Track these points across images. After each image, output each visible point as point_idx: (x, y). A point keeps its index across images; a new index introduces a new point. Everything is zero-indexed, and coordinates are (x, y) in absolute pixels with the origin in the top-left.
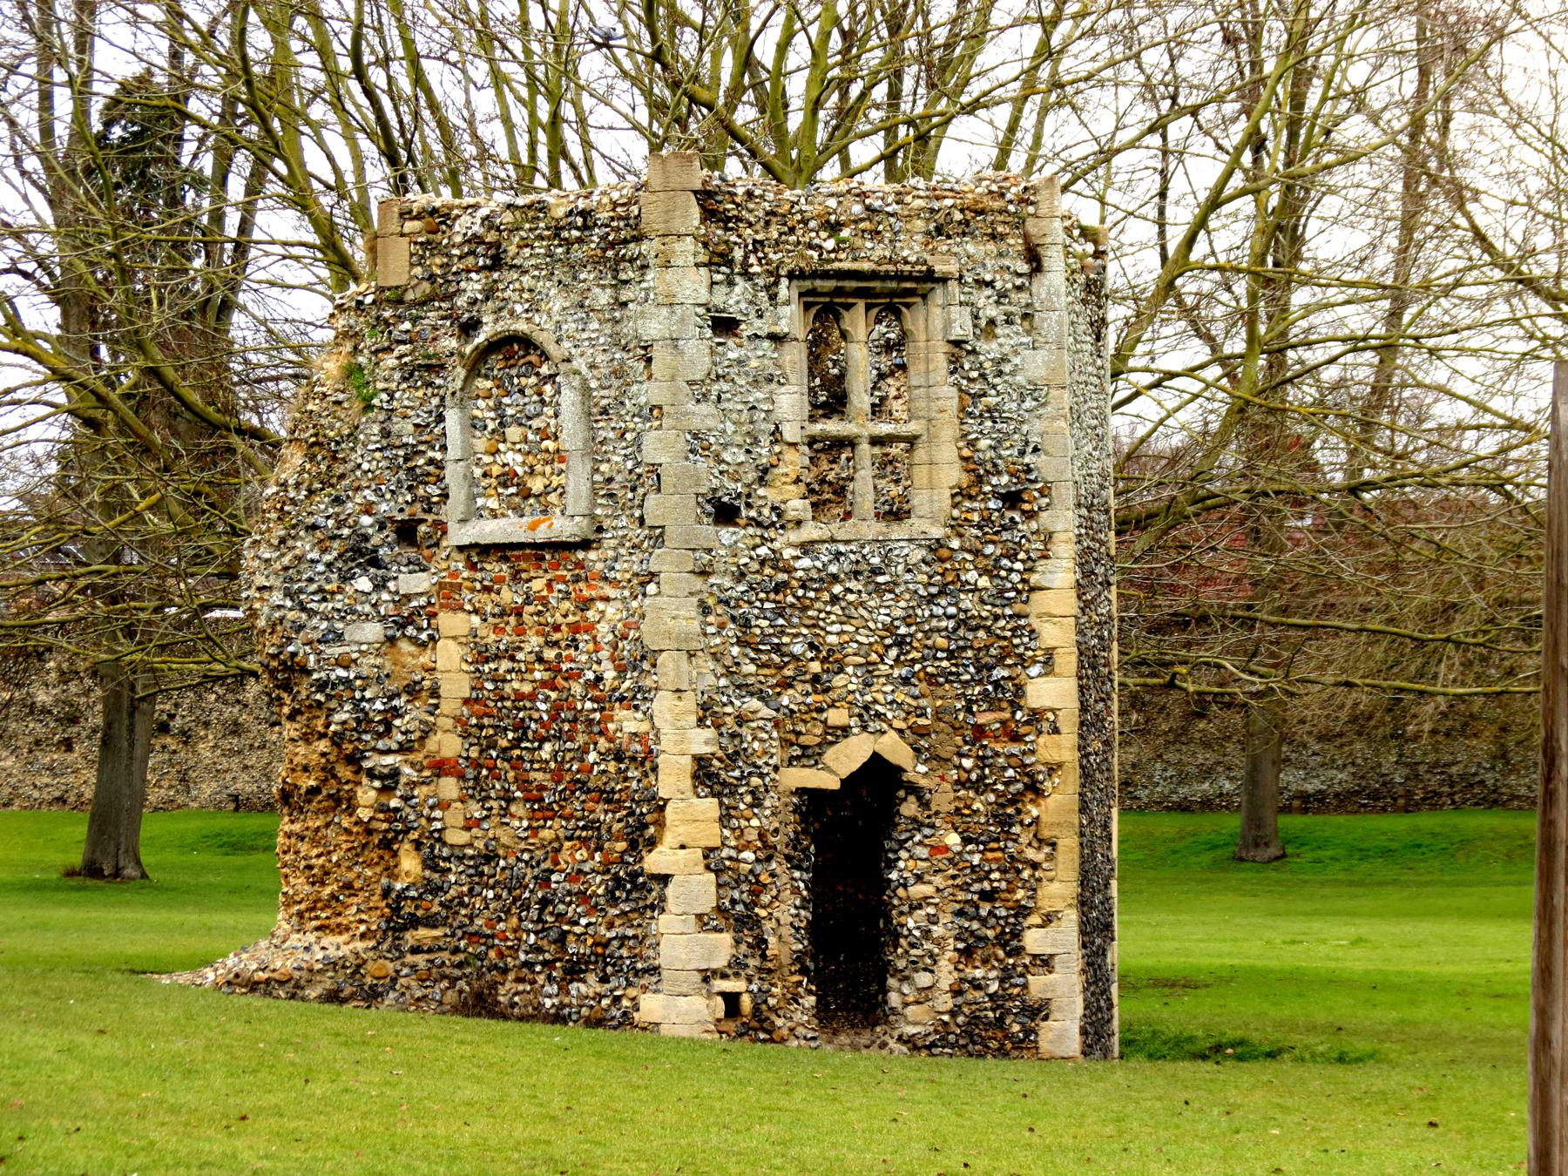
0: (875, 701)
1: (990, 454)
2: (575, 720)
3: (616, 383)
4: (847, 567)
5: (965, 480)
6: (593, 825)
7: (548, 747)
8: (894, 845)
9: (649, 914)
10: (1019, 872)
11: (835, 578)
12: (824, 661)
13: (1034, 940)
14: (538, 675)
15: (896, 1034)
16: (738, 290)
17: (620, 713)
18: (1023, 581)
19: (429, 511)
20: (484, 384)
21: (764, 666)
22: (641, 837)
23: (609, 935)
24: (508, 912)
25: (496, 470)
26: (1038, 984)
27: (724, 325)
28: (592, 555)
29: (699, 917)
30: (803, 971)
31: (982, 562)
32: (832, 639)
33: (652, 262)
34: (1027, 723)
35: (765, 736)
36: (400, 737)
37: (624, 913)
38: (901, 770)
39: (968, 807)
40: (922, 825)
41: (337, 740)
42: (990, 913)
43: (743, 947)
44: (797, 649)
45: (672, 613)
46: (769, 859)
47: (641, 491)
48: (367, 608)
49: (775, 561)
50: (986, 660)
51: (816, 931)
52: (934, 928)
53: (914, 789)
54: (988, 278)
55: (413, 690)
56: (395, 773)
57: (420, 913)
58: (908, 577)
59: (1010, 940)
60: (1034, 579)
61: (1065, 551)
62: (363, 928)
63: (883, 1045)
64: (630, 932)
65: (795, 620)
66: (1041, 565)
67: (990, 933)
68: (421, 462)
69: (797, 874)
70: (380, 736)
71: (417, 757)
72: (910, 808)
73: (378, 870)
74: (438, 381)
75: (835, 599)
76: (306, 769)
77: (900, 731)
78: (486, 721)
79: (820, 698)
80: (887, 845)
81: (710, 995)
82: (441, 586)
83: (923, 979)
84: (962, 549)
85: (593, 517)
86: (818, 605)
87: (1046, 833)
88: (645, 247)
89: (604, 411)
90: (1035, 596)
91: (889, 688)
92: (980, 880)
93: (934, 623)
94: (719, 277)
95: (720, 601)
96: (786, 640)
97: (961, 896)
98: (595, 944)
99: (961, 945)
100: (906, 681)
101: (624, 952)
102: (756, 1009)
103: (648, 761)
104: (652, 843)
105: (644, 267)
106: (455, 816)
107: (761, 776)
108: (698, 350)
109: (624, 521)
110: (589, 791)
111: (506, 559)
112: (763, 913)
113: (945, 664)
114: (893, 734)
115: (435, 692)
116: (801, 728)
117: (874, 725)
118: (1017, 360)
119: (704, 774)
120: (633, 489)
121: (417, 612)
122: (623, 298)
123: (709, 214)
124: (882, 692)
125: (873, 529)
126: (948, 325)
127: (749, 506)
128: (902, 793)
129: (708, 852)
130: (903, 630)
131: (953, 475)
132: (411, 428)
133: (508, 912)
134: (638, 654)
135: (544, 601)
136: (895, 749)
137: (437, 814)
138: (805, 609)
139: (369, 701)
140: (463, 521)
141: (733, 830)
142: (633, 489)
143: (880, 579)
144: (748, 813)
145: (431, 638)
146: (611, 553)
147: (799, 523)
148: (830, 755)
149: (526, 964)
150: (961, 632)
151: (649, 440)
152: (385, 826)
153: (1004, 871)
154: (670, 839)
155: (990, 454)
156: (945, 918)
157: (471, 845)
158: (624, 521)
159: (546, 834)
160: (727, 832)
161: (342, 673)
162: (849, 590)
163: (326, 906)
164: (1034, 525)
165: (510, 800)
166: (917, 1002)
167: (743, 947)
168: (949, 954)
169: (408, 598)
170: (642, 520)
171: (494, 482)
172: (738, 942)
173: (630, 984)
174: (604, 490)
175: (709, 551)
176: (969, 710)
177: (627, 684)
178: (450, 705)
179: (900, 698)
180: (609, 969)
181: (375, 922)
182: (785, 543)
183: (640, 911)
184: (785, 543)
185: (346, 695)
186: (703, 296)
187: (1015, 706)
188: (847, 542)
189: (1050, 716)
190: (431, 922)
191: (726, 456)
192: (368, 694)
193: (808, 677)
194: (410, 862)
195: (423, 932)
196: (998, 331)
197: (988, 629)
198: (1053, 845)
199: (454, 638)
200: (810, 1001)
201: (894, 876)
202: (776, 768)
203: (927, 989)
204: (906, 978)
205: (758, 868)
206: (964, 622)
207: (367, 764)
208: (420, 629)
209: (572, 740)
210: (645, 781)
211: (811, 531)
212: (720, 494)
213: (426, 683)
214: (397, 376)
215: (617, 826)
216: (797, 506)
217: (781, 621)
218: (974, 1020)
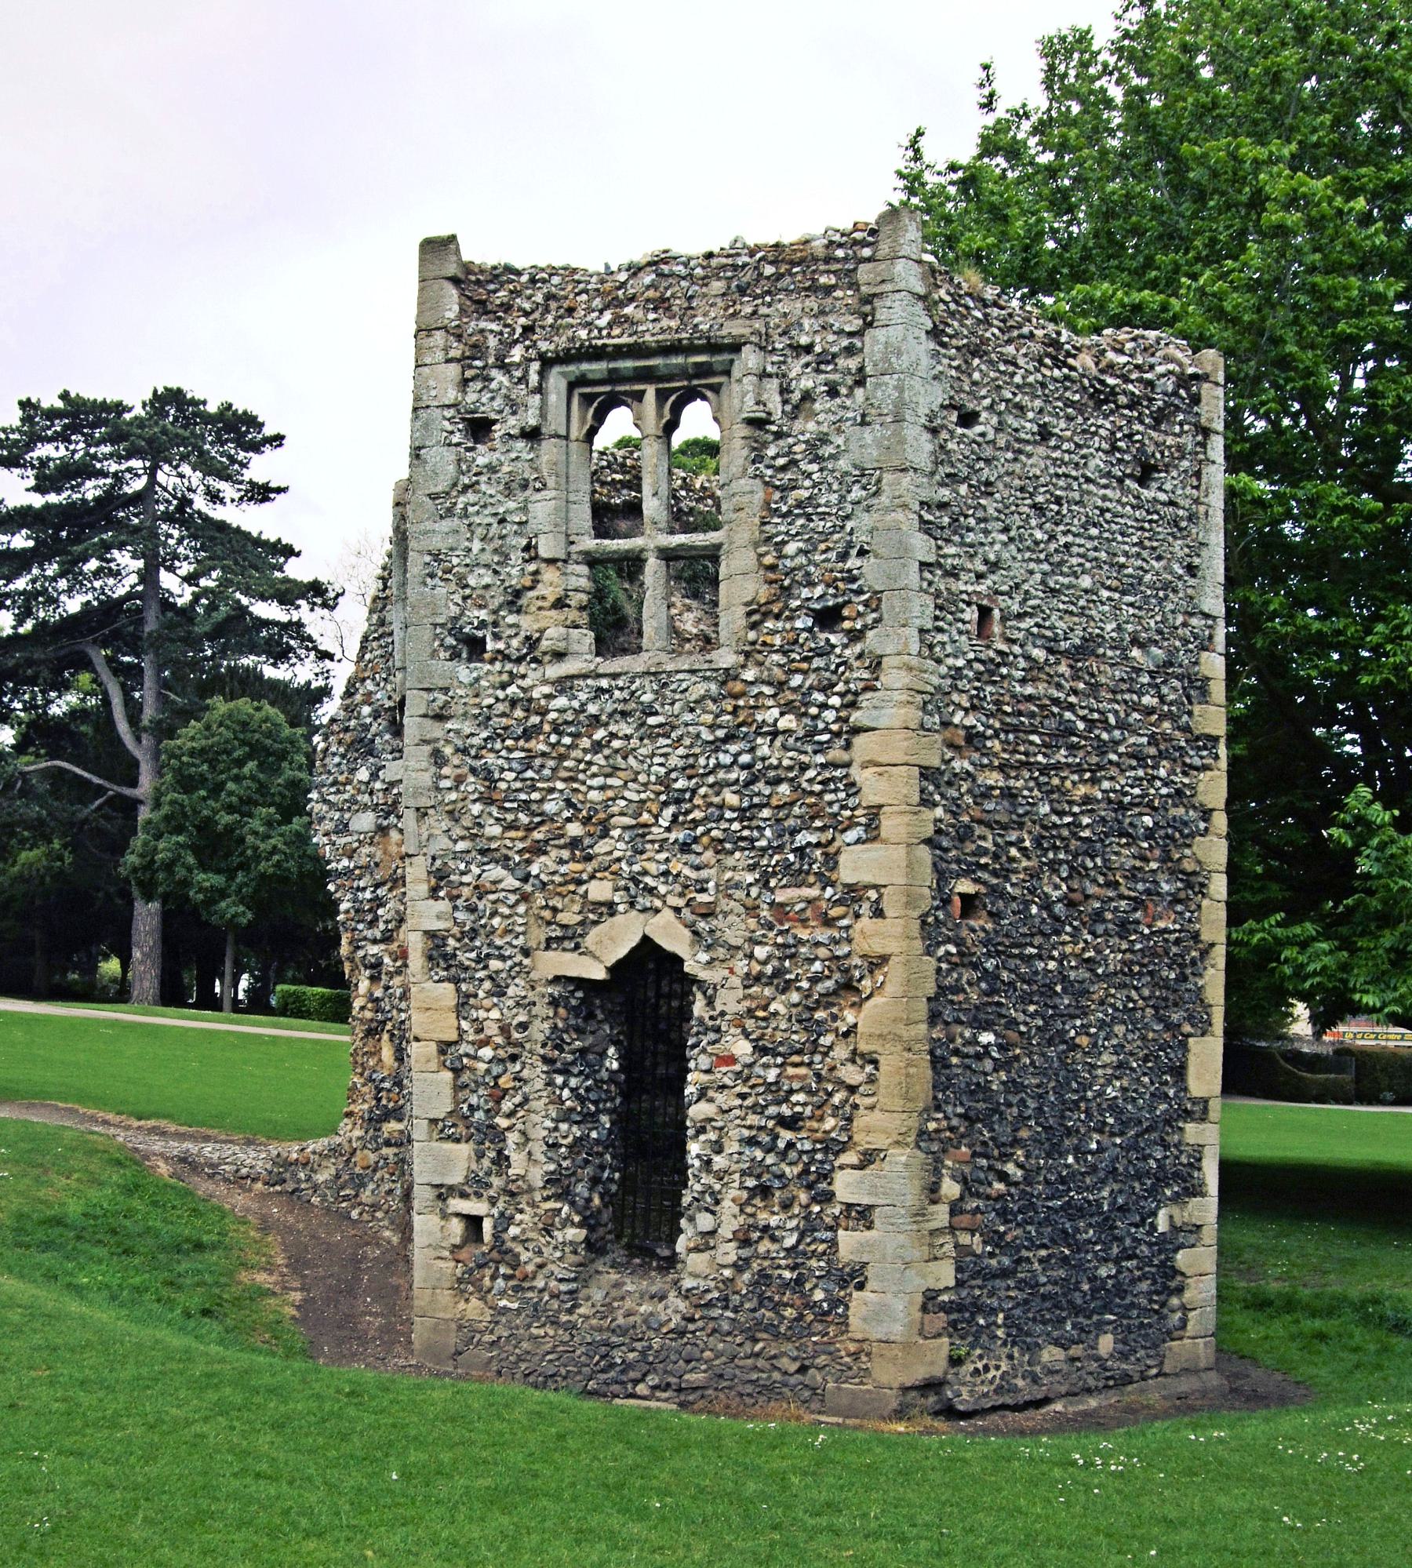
0: (645, 873)
5: (764, 593)
11: (595, 721)
12: (586, 821)
13: (846, 1186)
27: (479, 429)
29: (434, 1121)
30: (565, 1195)
32: (594, 795)
44: (550, 807)
49: (528, 704)
50: (794, 830)
52: (717, 1159)
60: (856, 717)
72: (699, 1008)
75: (597, 747)
77: (677, 910)
79: (578, 867)
81: (445, 1216)
83: (705, 1221)
87: (863, 1047)
90: (859, 741)
92: (779, 1103)
96: (535, 796)
100: (685, 848)
102: (496, 1236)
114: (667, 915)
116: (557, 902)
117: (644, 901)
118: (840, 441)
119: (438, 952)
129: (444, 1047)
136: (673, 937)
138: (562, 758)
160: (465, 1025)
168: (733, 1193)
172: (480, 1156)
175: (445, 690)
179: (675, 867)
184: (536, 681)
186: (452, 395)
198: (875, 1062)
217: (530, 774)
218: (763, 1277)
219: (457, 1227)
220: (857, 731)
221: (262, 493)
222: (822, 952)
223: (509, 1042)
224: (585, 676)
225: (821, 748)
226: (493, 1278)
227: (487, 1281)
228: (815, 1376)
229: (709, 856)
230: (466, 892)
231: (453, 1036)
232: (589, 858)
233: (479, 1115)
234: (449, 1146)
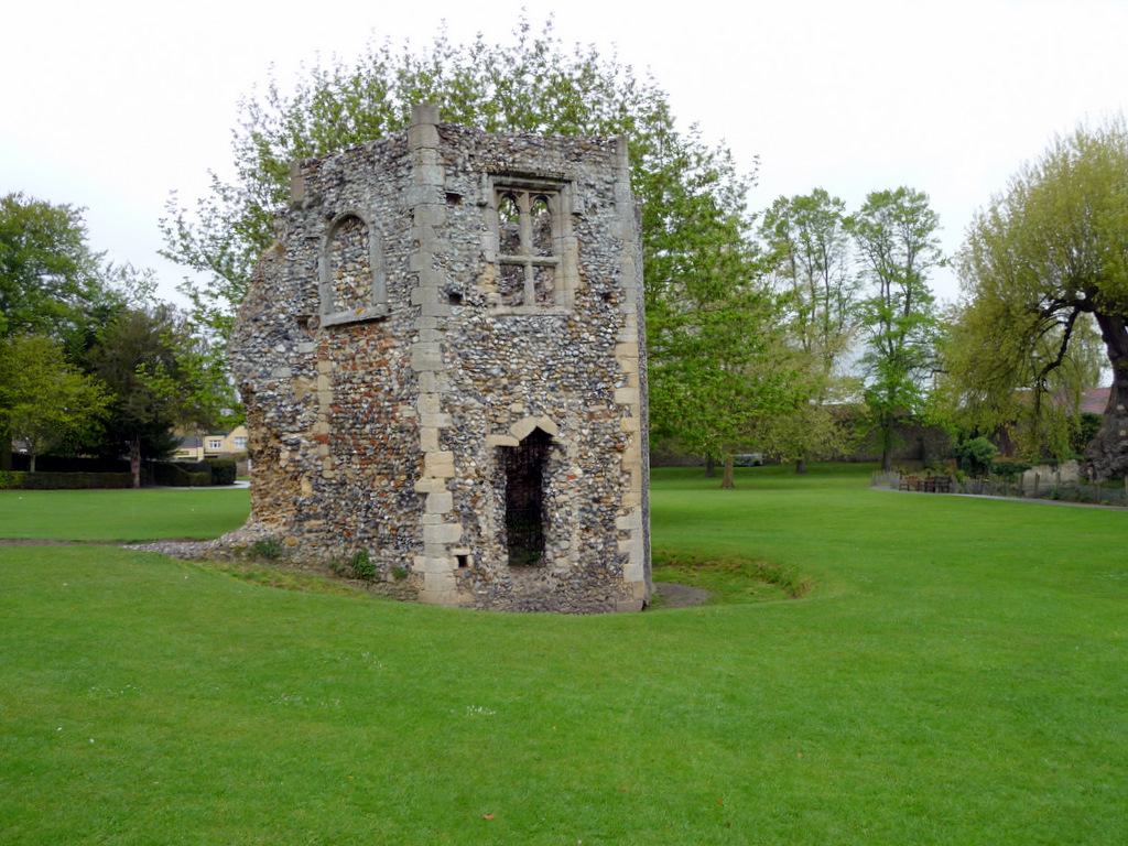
0: (537, 400)
1: (594, 273)
2: (380, 413)
3: (397, 231)
4: (521, 329)
5: (582, 285)
6: (390, 467)
7: (368, 427)
8: (548, 475)
9: (418, 514)
10: (612, 487)
11: (514, 335)
12: (510, 378)
13: (621, 522)
14: (362, 390)
15: (551, 573)
16: (460, 179)
17: (401, 407)
18: (612, 338)
19: (313, 311)
20: (336, 244)
21: (477, 380)
22: (413, 473)
23: (398, 525)
24: (351, 512)
25: (343, 287)
26: (623, 545)
27: (453, 198)
28: (387, 325)
29: (444, 515)
30: (501, 542)
31: (591, 328)
32: (513, 366)
33: (413, 164)
34: (615, 411)
35: (478, 418)
36: (300, 425)
37: (406, 513)
38: (551, 436)
39: (586, 455)
40: (561, 464)
41: (269, 426)
42: (598, 509)
43: (468, 531)
44: (495, 371)
45: (428, 351)
46: (481, 483)
47: (409, 287)
48: (283, 360)
49: (482, 325)
50: (596, 383)
51: (510, 521)
52: (570, 518)
53: (557, 445)
54: (592, 183)
55: (306, 401)
56: (298, 443)
57: (311, 512)
58: (553, 335)
59: (608, 524)
61: (632, 322)
62: (284, 520)
63: (544, 579)
64: (408, 523)
65: (493, 356)
66: (621, 331)
67: (598, 520)
68: (309, 286)
69: (497, 491)
70: (290, 424)
71: (309, 434)
72: (556, 455)
73: (292, 491)
74: (316, 246)
75: (514, 346)
76: (257, 441)
77: (550, 415)
78: (340, 415)
79: (507, 398)
80: (544, 475)
81: (450, 557)
82: (319, 348)
84: (581, 321)
85: (386, 303)
86: (505, 348)
87: (626, 468)
88: (410, 157)
89: (391, 247)
90: (619, 346)
91: (544, 393)
92: (592, 492)
93: (567, 359)
94: (450, 172)
95: (452, 345)
96: (488, 366)
97: (583, 501)
98: (392, 529)
99: (584, 526)
100: (553, 389)
101: (406, 534)
102: (476, 564)
103: (415, 432)
104: (418, 476)
105: (410, 168)
106: (327, 464)
107: (476, 439)
108: (440, 210)
109: (402, 305)
110: (388, 449)
111: (347, 331)
112: (479, 512)
113: (573, 380)
114: (546, 418)
115: (317, 402)
116: (497, 413)
117: (537, 412)
118: (608, 226)
119: (444, 437)
120: (406, 287)
121: (308, 362)
122: (399, 186)
123: (444, 139)
124: (541, 394)
125: (534, 309)
126: (572, 206)
127: (467, 294)
128: (551, 448)
129: (448, 480)
130: (551, 362)
131: (575, 283)
132: (304, 270)
133: (351, 512)
134: (409, 375)
135: (365, 352)
136: (548, 425)
137: (319, 463)
138: (499, 350)
139: (285, 406)
140: (327, 314)
141: (462, 468)
142: (406, 287)
143: (539, 335)
144: (469, 459)
145: (315, 375)
146: (396, 323)
147: (495, 305)
148: (513, 428)
149: (360, 539)
150: (581, 364)
151: (413, 259)
152: (293, 469)
153: (604, 487)
154: (427, 474)
155: (594, 273)
156: (575, 513)
157: (334, 478)
158: (402, 305)
159: (368, 472)
160: (458, 470)
161: (271, 393)
162: (522, 341)
163: (268, 509)
164: (617, 310)
165: (352, 455)
166: (561, 556)
167: (468, 531)
168: (577, 531)
169: (303, 354)
170: (410, 303)
171: (341, 293)
172: (465, 528)
173: (409, 551)
174: (393, 289)
175: (445, 318)
176: (586, 404)
177: (405, 391)
178: (324, 408)
179: (550, 397)
180: (399, 543)
181: (290, 516)
182: (487, 315)
183: (413, 512)
184: (487, 315)
185: (273, 404)
186: (441, 181)
187: (609, 402)
188: (521, 316)
189: (627, 408)
190: (316, 516)
191: (455, 268)
192: (284, 403)
193: (501, 386)
194: (306, 487)
195: (313, 522)
196: (598, 210)
197: (594, 362)
198: (629, 473)
199: (325, 374)
200: (506, 557)
201: (548, 491)
202: (484, 435)
203: (566, 551)
204: (556, 544)
205: (475, 489)
206: (583, 359)
207: (283, 438)
208: (310, 370)
209: (379, 422)
210: (414, 443)
211: (501, 310)
212: (451, 287)
213: (313, 398)
214: (296, 243)
215: (401, 467)
216: (493, 296)
217: (486, 357)
218: (591, 564)
219: (456, 560)
220: (617, 343)
221: (425, 49)
222: (609, 431)
223: (479, 476)
224: (508, 315)
225: (605, 349)
226: (474, 582)
227: (471, 583)
228: (612, 600)
229: (562, 392)
230: (458, 409)
231: (451, 475)
232: (511, 394)
233: (466, 510)
234: (452, 525)
